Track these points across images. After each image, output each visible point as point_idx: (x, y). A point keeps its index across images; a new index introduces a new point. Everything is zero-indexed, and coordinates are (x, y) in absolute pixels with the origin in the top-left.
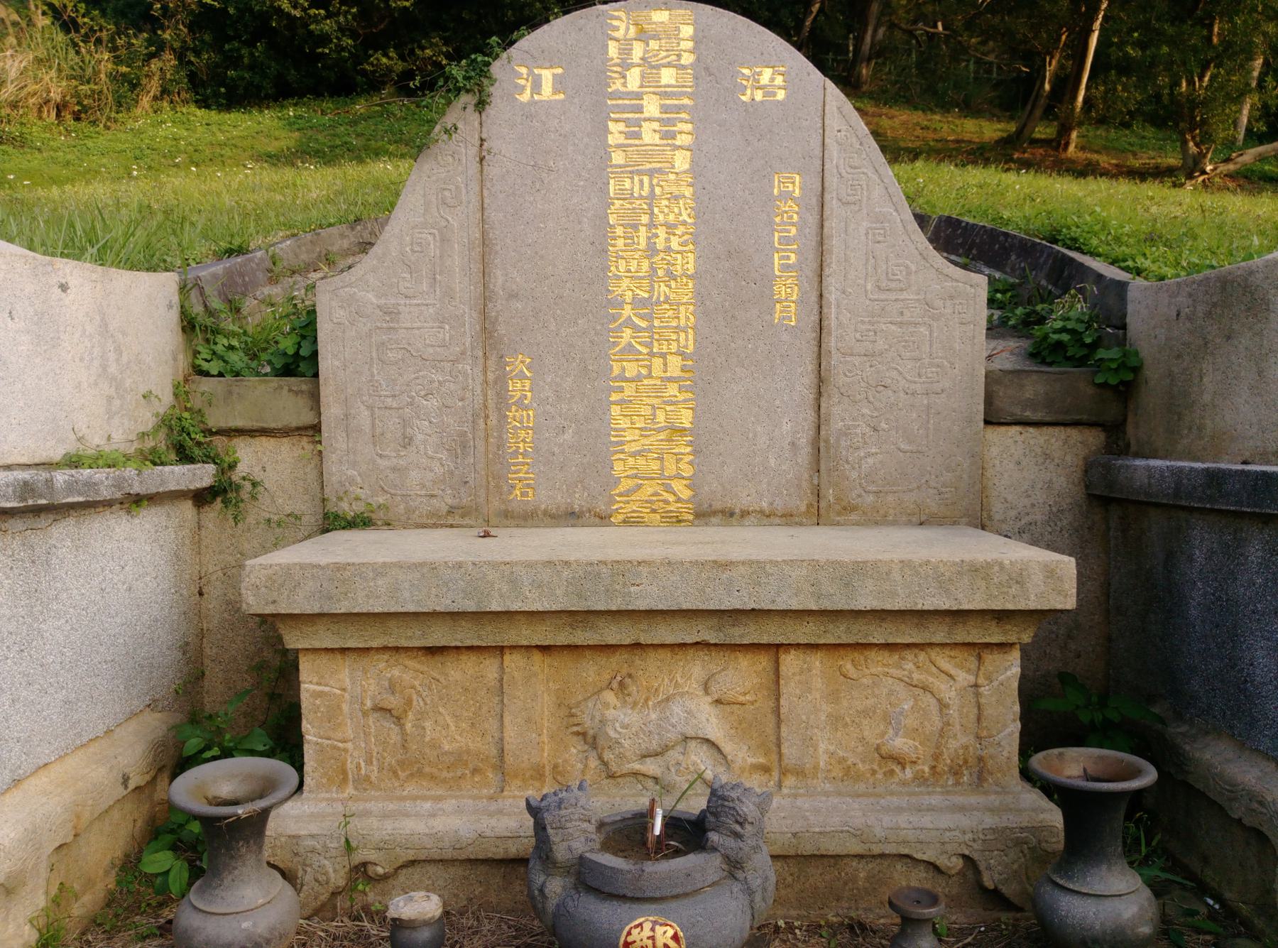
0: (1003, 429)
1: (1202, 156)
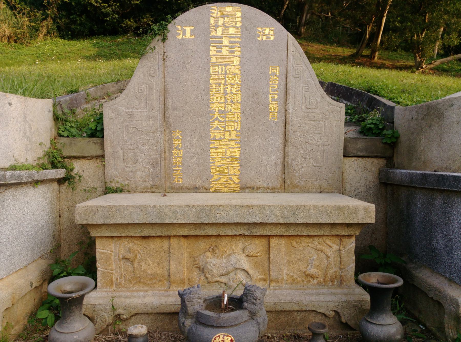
0: (350, 158)
1: (422, 62)
